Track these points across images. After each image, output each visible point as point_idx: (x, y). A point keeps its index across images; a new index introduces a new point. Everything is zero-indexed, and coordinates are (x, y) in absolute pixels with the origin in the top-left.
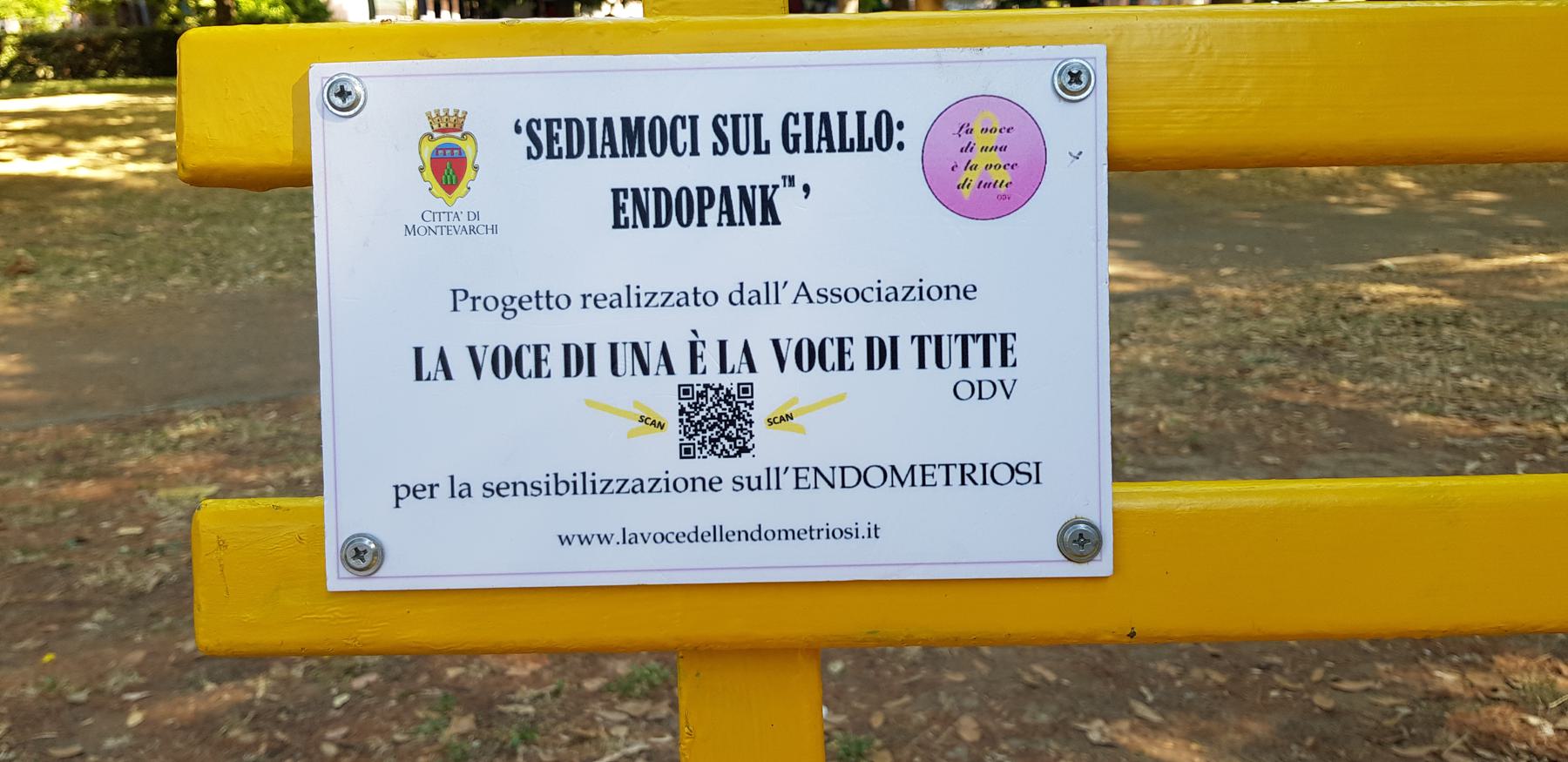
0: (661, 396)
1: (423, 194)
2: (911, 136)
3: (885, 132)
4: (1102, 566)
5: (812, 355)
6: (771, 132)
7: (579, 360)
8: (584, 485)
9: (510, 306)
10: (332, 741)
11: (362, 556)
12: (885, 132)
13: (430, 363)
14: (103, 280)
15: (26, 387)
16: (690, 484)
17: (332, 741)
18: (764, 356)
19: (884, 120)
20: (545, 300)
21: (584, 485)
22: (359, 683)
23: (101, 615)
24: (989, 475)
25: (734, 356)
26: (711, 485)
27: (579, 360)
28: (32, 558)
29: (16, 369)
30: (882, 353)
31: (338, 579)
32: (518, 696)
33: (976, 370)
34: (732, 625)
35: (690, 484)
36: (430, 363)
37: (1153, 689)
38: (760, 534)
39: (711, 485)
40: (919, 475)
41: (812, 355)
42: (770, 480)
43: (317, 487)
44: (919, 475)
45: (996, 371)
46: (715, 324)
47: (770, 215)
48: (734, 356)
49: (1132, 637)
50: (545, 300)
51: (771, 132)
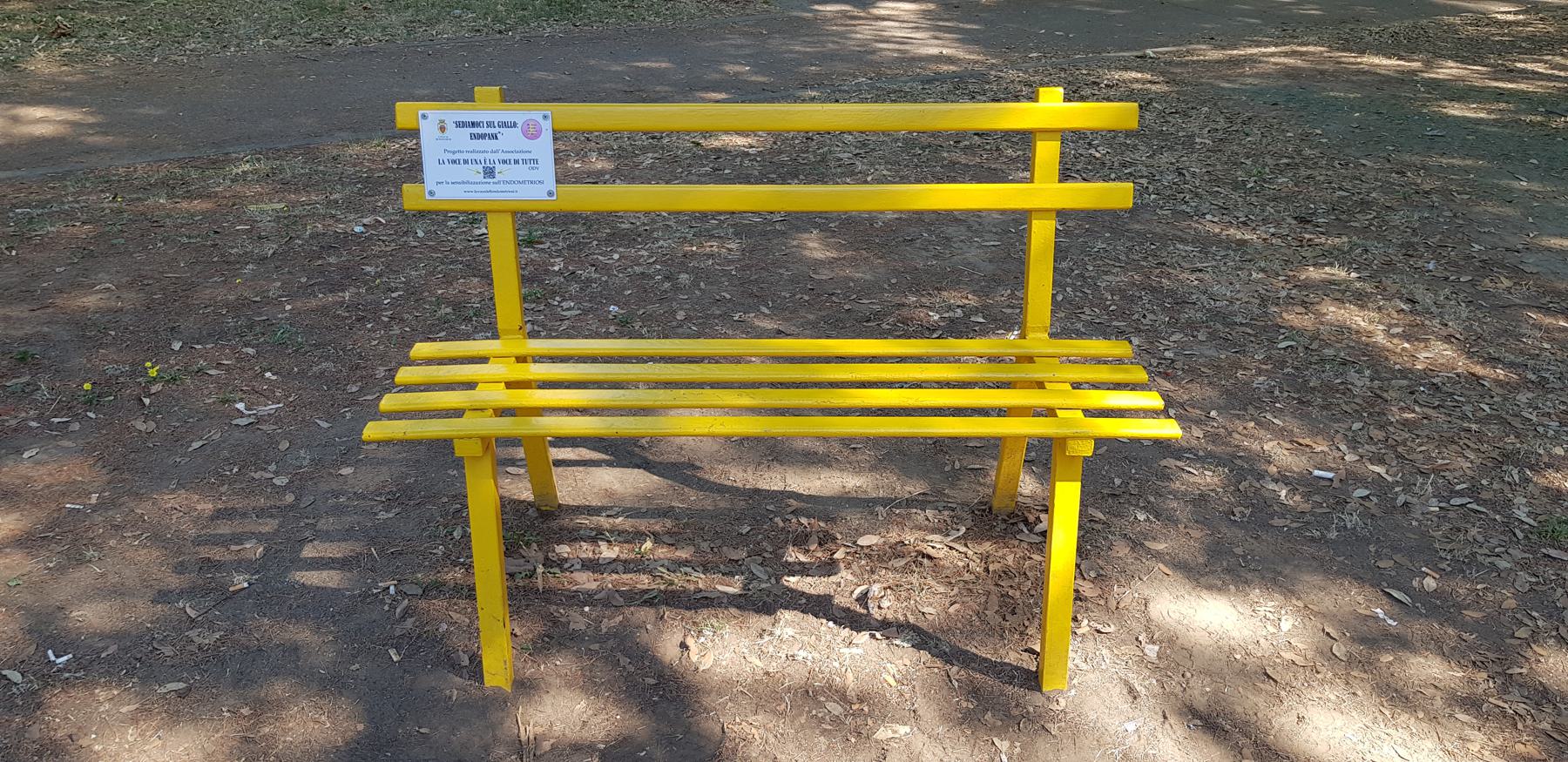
0: (480, 168)
1: (439, 133)
2: (519, 125)
3: (515, 125)
4: (555, 198)
5: (505, 162)
6: (496, 124)
7: (466, 162)
8: (468, 182)
9: (454, 153)
10: (386, 316)
11: (431, 193)
12: (515, 125)
13: (441, 162)
14: (133, 44)
15: (106, 134)
16: (486, 183)
17: (386, 316)
18: (497, 162)
19: (515, 122)
20: (459, 151)
21: (468, 182)
22: (393, 295)
23: (250, 266)
24: (535, 182)
25: (492, 162)
26: (489, 183)
27: (466, 162)
28: (192, 241)
29: (91, 120)
30: (516, 162)
31: (428, 197)
32: (473, 300)
33: (532, 165)
34: (495, 207)
35: (486, 183)
36: (441, 162)
37: (773, 301)
38: (498, 192)
39: (489, 183)
40: (524, 182)
41: (505, 162)
42: (499, 182)
43: (424, 183)
44: (524, 182)
45: (536, 165)
46: (489, 156)
47: (497, 138)
48: (492, 162)
49: (1074, 388)
50: (459, 151)
51: (496, 124)
